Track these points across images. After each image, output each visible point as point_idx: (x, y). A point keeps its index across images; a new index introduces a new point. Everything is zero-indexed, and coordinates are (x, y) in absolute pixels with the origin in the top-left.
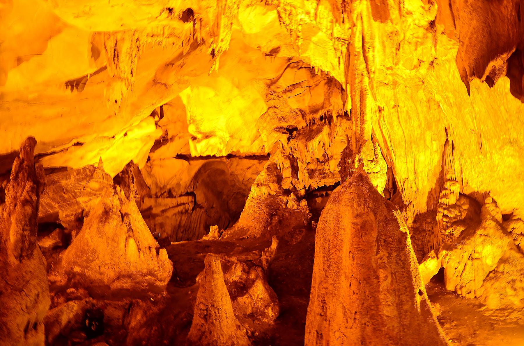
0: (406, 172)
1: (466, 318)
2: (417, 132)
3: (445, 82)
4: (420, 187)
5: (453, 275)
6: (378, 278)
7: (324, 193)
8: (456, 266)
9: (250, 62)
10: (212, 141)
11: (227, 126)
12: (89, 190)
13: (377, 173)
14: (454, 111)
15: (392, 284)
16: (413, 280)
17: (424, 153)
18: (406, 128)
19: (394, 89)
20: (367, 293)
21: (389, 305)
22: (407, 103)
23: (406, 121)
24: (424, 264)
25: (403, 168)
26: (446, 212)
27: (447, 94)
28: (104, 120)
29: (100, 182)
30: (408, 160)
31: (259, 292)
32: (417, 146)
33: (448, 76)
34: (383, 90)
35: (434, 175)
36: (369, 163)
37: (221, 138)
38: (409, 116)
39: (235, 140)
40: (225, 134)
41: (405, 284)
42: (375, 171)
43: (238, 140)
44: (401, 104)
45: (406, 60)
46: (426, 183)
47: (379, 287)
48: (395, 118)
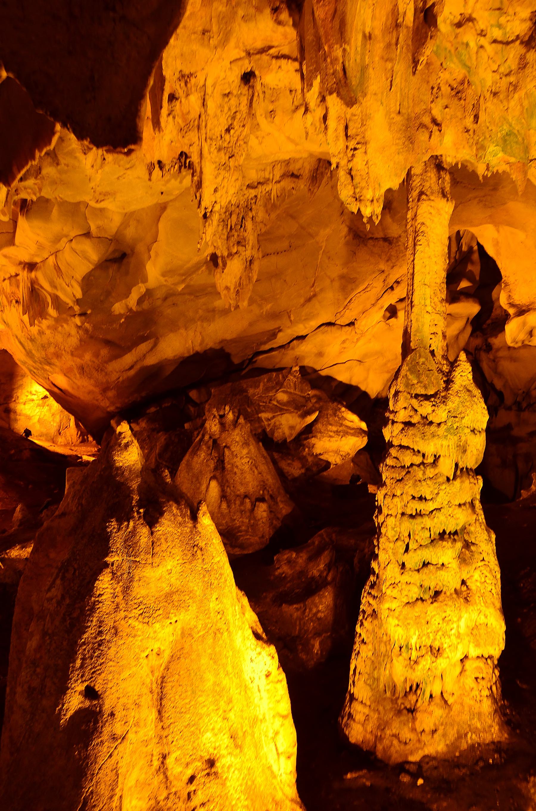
12: (276, 403)
13: (439, 424)
16: (74, 662)
28: (303, 305)
29: (291, 393)
31: (321, 607)
42: (436, 420)
45: (505, 141)
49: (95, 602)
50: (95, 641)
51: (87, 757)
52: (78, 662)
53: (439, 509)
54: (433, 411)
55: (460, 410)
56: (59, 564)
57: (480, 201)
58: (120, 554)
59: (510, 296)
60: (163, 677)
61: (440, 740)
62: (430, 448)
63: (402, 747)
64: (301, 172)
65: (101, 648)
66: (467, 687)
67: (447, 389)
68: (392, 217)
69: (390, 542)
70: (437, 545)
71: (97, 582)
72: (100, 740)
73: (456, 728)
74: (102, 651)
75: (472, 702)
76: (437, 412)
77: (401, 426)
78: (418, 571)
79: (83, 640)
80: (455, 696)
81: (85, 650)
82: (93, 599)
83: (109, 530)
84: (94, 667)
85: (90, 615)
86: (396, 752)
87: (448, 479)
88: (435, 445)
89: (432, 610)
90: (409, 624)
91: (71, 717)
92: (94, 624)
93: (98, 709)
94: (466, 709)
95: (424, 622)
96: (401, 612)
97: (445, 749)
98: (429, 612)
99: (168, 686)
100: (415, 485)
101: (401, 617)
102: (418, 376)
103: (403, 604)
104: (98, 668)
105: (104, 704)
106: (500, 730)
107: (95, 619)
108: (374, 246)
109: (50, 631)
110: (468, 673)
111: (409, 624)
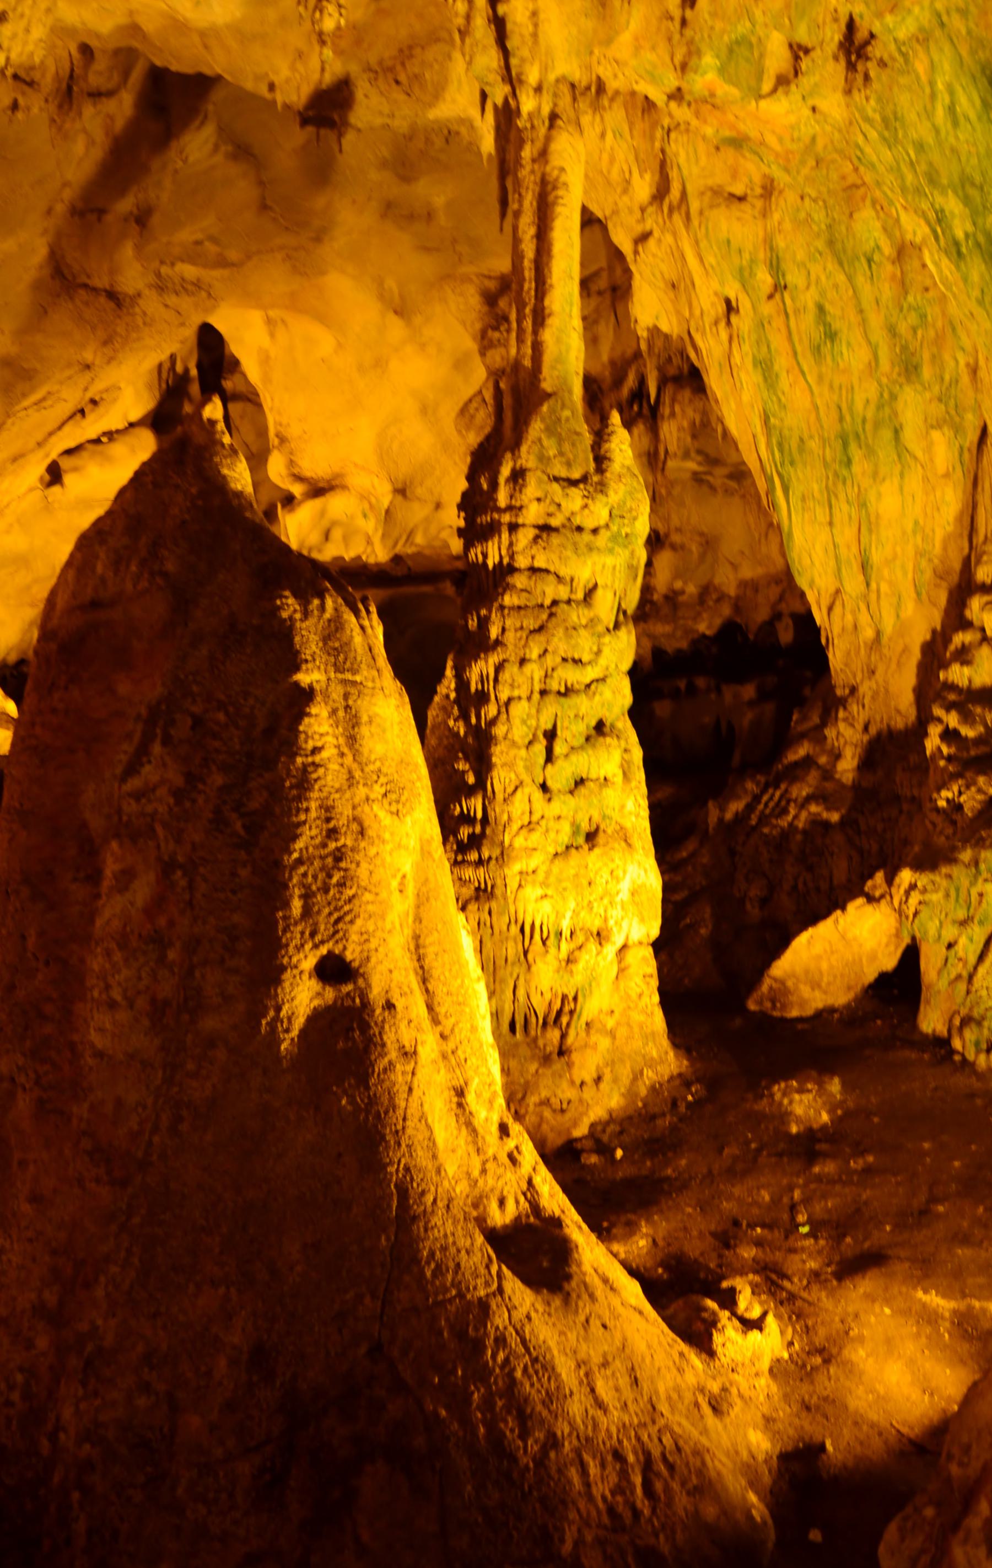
0: (832, 563)
1: (926, 1145)
2: (865, 394)
3: (920, 147)
4: (888, 625)
5: (939, 972)
6: (94, 877)
7: (682, 684)
8: (950, 933)
9: (430, 216)
10: (337, 504)
11: (383, 453)
13: (595, 531)
14: (975, 277)
15: (150, 911)
16: (287, 905)
17: (896, 480)
18: (820, 378)
19: (764, 215)
20: (31, 941)
21: (112, 1005)
22: (815, 269)
23: (817, 351)
24: (837, 921)
25: (818, 548)
26: (953, 720)
27: (939, 200)
30: (836, 511)
32: (870, 452)
33: (929, 114)
34: (724, 226)
35: (940, 575)
36: (556, 486)
37: (364, 497)
38: (827, 325)
39: (416, 506)
40: (376, 481)
41: (237, 918)
42: (589, 524)
43: (431, 506)
44: (794, 277)
45: (731, 51)
46: (909, 608)
47: (92, 921)
48: (777, 341)
49: (305, 766)
50: (323, 852)
51: (373, 1101)
52: (297, 906)
53: (603, 680)
54: (586, 506)
55: (628, 505)
56: (144, 711)
57: (289, 257)
58: (322, 667)
59: (291, 461)
60: (417, 938)
61: (612, 1089)
62: (583, 570)
63: (559, 1118)
64: (37, 76)
65: (343, 865)
66: (634, 996)
67: (600, 470)
68: (138, 248)
69: (519, 748)
70: (598, 745)
71: (306, 720)
72: (386, 1060)
73: (628, 1065)
74: (346, 870)
75: (642, 1018)
76: (592, 507)
77: (531, 533)
78: (571, 792)
79: (295, 855)
80: (617, 1014)
81: (305, 875)
82: (299, 760)
83: (285, 615)
84: (337, 909)
85: (299, 798)
86: (552, 1130)
87: (608, 630)
88: (594, 564)
89: (594, 859)
90: (565, 889)
91: (303, 1032)
92: (313, 814)
93: (358, 1001)
94: (636, 1030)
95: (585, 883)
96: (548, 873)
97: (622, 1102)
98: (590, 865)
99: (430, 951)
100: (568, 636)
101: (552, 879)
102: (560, 441)
103: (550, 857)
104: (346, 908)
105: (369, 986)
106: (676, 1056)
107: (313, 805)
108: (87, 304)
109: (180, 859)
110: (631, 970)
111: (565, 889)
